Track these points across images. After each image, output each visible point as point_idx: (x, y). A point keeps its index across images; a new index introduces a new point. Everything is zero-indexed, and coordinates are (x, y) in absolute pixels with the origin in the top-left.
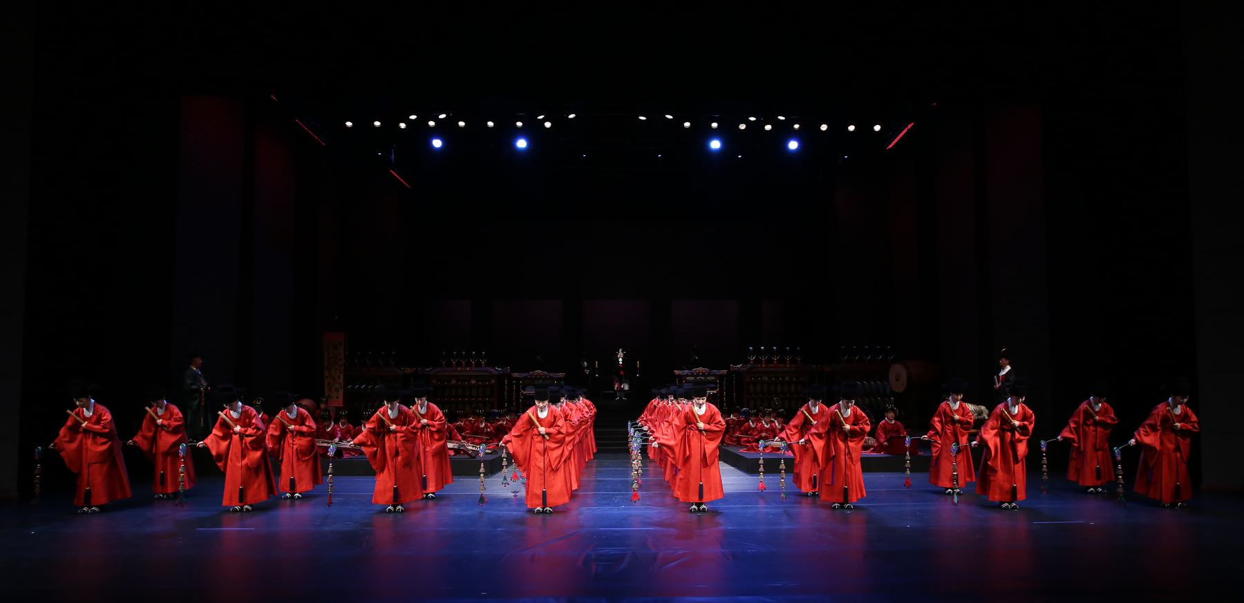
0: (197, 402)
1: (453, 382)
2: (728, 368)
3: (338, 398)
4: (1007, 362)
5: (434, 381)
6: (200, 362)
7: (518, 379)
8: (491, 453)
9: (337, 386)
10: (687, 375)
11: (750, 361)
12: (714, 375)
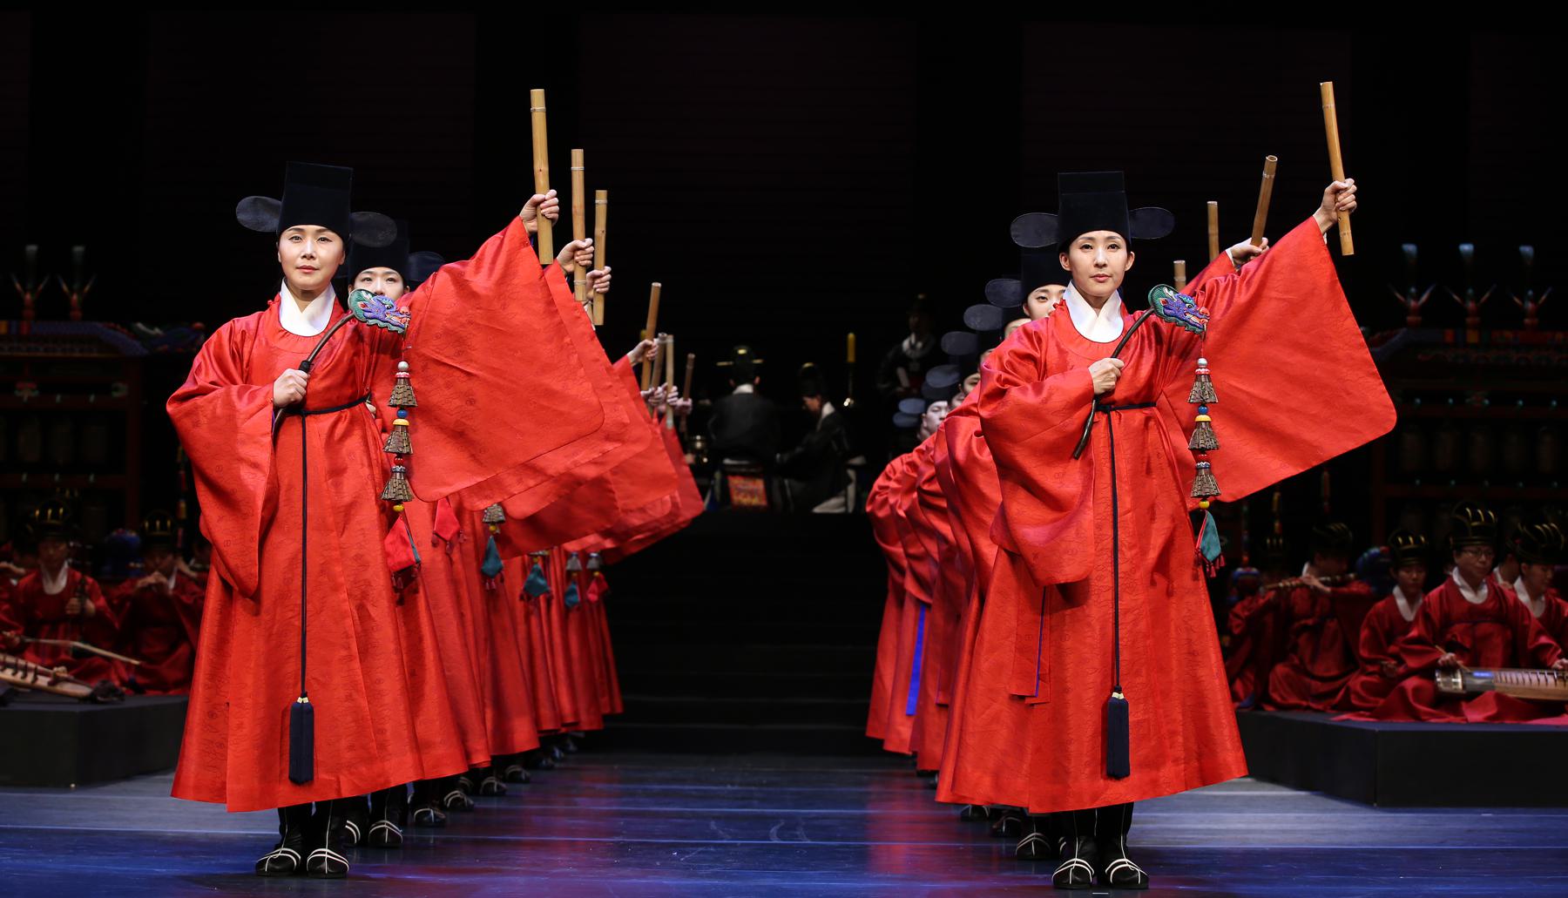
11: (1405, 310)
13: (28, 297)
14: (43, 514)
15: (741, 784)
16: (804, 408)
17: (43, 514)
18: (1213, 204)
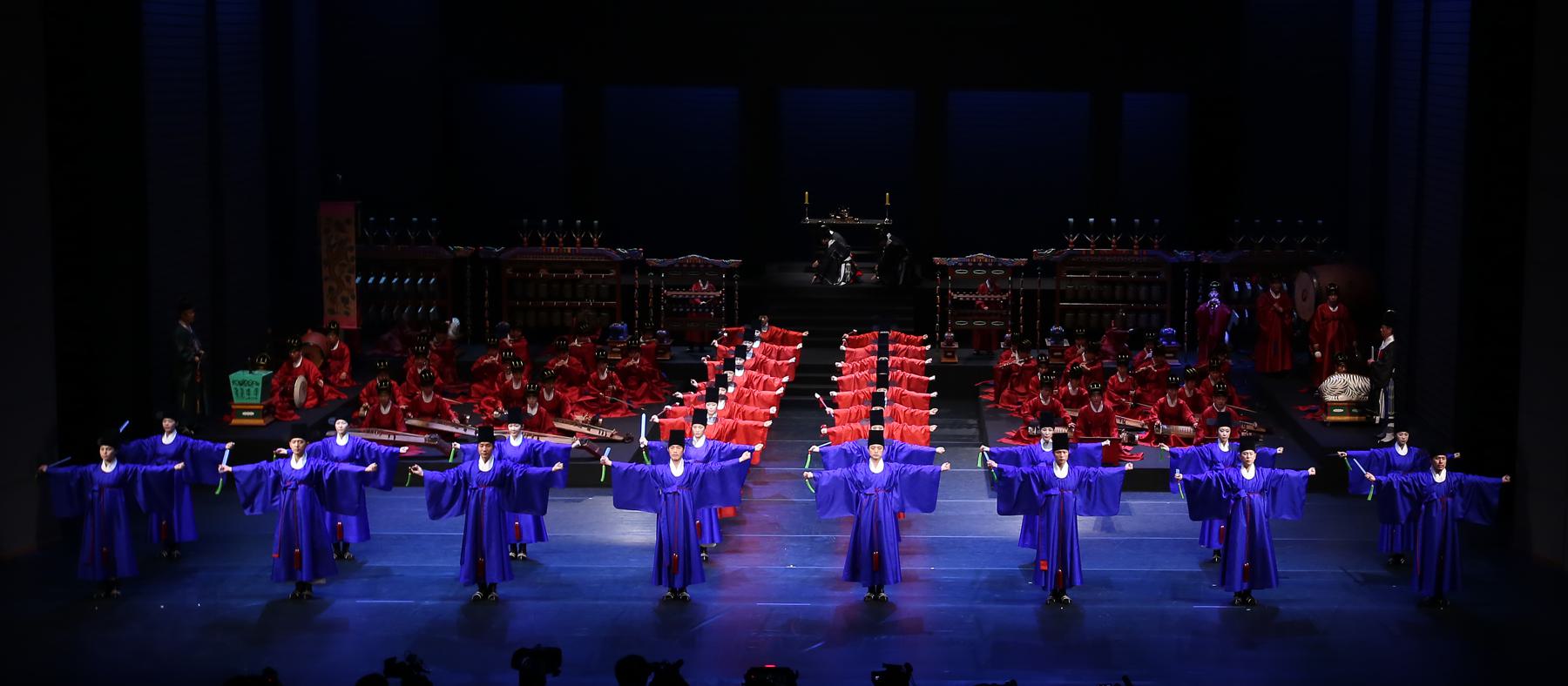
0: (188, 378)
1: (542, 273)
2: (1029, 255)
3: (347, 314)
4: (1389, 331)
5: (509, 271)
6: (193, 315)
7: (657, 270)
8: (623, 441)
9: (345, 293)
10: (956, 267)
11: (1068, 242)
12: (1004, 267)
13: (525, 239)
14: (598, 354)
15: (1267, 523)
16: (310, 331)
17: (598, 354)
18: (888, 204)
